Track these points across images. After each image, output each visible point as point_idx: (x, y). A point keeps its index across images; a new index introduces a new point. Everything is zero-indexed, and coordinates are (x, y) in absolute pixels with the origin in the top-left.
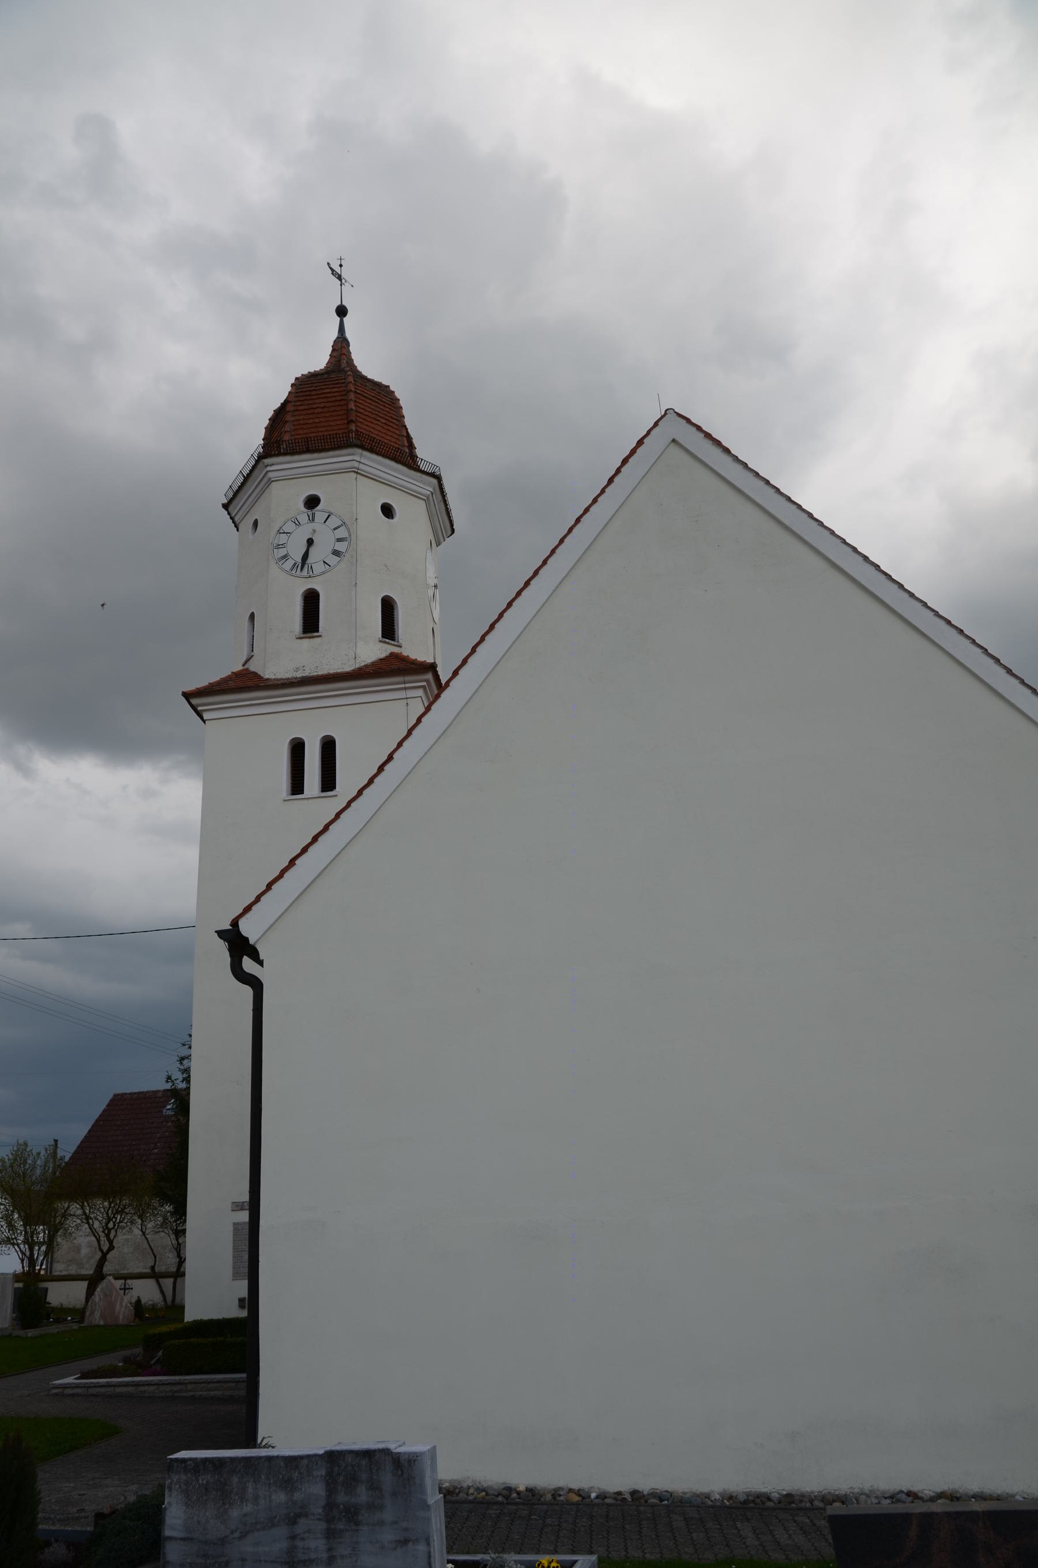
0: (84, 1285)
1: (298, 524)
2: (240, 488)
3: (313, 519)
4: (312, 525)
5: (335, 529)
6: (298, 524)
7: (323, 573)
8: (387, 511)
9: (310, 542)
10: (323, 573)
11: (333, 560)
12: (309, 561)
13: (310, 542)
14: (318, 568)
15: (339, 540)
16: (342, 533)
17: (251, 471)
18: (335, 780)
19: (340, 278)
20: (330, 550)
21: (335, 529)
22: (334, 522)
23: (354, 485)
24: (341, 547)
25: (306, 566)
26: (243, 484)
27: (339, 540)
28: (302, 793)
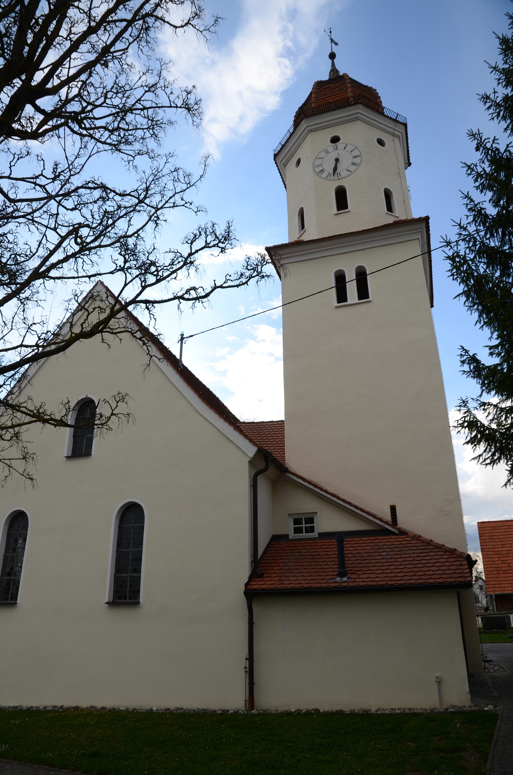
0: (116, 295)
1: (327, 152)
2: (279, 151)
3: (337, 148)
4: (337, 151)
5: (351, 151)
6: (327, 152)
7: (357, 169)
8: (381, 142)
9: (337, 160)
10: (357, 169)
11: (353, 168)
12: (338, 171)
13: (337, 160)
14: (344, 173)
15: (354, 157)
16: (356, 153)
17: (286, 142)
18: (346, 296)
19: (332, 40)
20: (350, 162)
21: (351, 151)
22: (349, 148)
23: (357, 132)
24: (357, 160)
25: (336, 174)
26: (281, 149)
27: (354, 157)
28: (346, 301)
